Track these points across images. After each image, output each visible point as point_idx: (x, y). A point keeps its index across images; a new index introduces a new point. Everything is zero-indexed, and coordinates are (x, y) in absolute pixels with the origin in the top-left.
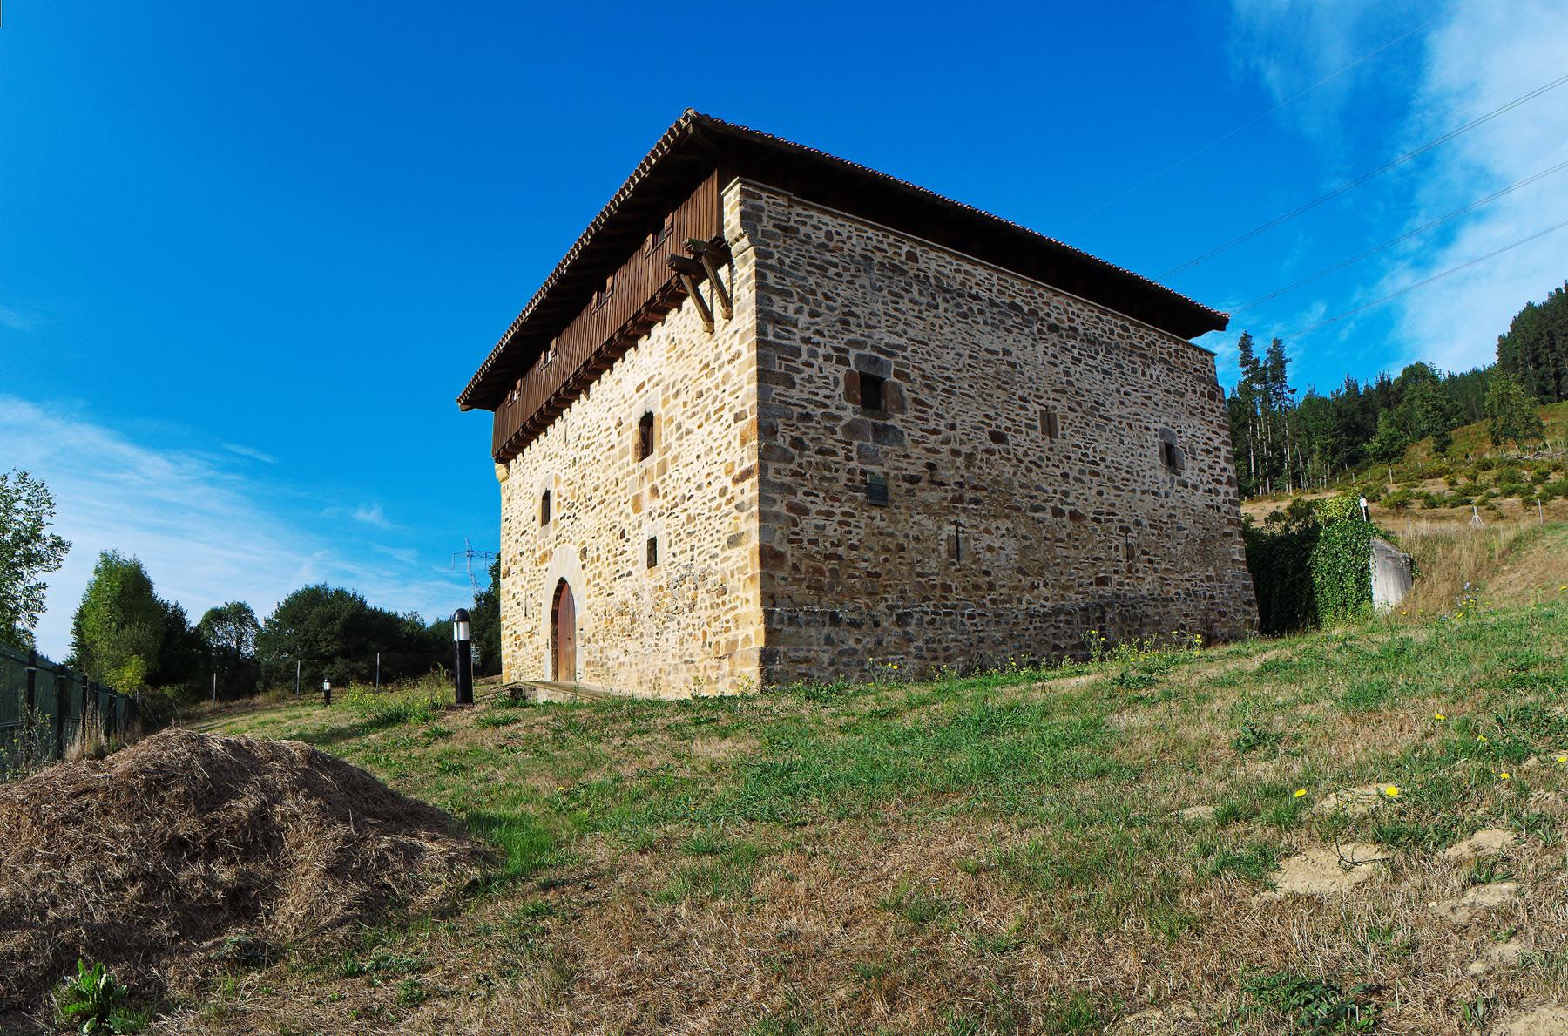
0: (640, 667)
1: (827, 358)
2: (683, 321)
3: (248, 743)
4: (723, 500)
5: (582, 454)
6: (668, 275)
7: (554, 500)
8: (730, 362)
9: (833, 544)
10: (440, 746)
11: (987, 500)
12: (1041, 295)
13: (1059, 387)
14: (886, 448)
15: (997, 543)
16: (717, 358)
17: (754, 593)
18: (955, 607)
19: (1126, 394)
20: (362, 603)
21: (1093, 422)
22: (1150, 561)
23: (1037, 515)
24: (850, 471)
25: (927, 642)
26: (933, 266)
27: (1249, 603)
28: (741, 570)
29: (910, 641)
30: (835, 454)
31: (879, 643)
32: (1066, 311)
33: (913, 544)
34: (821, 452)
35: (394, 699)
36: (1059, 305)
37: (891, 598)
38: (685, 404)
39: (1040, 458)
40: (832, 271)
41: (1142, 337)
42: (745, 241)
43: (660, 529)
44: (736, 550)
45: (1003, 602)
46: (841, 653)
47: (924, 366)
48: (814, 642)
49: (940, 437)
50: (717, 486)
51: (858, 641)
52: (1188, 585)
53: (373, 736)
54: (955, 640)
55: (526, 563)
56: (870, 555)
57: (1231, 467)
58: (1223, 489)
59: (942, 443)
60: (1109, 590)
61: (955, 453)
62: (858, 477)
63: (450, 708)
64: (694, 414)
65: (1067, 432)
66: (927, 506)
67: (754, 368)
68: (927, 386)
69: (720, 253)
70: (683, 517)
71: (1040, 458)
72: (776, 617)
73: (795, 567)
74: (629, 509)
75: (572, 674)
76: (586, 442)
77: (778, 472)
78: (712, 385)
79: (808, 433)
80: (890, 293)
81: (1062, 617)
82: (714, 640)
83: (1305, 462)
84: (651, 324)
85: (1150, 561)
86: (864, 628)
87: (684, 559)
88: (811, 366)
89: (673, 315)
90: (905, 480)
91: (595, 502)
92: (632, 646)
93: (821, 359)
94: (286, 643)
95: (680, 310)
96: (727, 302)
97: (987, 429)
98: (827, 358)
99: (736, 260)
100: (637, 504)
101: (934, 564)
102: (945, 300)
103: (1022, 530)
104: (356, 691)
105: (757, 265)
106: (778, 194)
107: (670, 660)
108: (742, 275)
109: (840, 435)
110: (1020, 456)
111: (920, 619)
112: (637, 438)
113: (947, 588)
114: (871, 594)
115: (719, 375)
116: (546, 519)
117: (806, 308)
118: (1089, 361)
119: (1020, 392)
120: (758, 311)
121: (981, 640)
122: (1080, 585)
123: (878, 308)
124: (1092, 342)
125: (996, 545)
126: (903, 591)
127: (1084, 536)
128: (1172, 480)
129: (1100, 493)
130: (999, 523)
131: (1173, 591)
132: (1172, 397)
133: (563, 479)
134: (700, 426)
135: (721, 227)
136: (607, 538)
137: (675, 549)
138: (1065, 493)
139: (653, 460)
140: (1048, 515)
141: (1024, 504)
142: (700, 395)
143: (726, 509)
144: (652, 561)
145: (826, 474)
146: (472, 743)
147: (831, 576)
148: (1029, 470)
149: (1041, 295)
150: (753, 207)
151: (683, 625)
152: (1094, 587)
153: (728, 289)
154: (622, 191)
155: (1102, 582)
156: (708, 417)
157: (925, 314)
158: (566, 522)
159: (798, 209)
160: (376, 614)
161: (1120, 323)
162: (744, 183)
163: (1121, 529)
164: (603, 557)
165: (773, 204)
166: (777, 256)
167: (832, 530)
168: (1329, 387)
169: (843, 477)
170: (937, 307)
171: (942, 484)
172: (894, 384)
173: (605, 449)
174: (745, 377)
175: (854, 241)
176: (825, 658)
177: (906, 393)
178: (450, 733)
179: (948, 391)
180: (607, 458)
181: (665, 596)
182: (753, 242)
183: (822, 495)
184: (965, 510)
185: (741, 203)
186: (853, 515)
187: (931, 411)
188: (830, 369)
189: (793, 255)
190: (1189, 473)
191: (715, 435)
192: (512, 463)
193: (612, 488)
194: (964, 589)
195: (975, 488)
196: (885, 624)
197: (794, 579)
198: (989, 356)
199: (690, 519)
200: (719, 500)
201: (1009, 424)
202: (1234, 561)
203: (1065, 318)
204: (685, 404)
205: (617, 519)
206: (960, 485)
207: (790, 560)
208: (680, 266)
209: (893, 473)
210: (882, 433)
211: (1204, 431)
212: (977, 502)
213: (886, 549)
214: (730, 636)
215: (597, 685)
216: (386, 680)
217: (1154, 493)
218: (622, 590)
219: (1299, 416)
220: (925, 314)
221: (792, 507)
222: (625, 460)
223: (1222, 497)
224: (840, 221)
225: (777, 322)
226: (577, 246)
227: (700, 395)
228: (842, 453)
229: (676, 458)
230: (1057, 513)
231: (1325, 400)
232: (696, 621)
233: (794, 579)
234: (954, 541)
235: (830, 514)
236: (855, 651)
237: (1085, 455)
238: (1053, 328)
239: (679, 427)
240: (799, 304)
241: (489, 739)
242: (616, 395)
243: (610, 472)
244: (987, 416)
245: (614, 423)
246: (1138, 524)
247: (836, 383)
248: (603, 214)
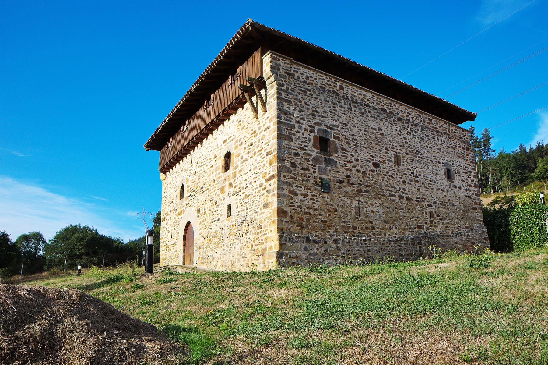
0: (222, 259)
1: (306, 130)
2: (245, 113)
3: (44, 290)
4: (261, 188)
5: (199, 169)
6: (239, 92)
7: (186, 189)
8: (265, 130)
9: (307, 208)
10: (139, 293)
11: (371, 191)
12: (395, 105)
13: (402, 144)
14: (330, 168)
15: (375, 210)
16: (259, 129)
17: (274, 228)
18: (358, 236)
19: (430, 148)
20: (96, 232)
21: (416, 159)
22: (441, 219)
23: (392, 198)
24: (315, 178)
25: (346, 251)
26: (350, 92)
27: (485, 239)
28: (269, 218)
29: (339, 250)
30: (309, 170)
31: (326, 250)
32: (405, 112)
33: (341, 209)
34: (303, 169)
35: (111, 273)
36: (403, 110)
37: (332, 231)
38: (245, 148)
39: (394, 174)
40: (308, 93)
41: (437, 124)
42: (272, 79)
43: (232, 200)
44: (267, 210)
45: (378, 235)
46: (311, 255)
47: (346, 134)
48: (298, 250)
49: (352, 164)
50: (258, 183)
51: (318, 249)
52: (457, 230)
53: (105, 288)
54: (358, 250)
55: (173, 215)
56: (323, 213)
57: (476, 180)
58: (472, 189)
59: (353, 167)
60: (422, 231)
61: (358, 171)
62: (318, 180)
63: (143, 275)
64: (249, 153)
65: (405, 163)
66: (346, 193)
67: (276, 133)
68: (347, 142)
69: (262, 83)
70: (243, 196)
71: (394, 174)
72: (283, 238)
73: (292, 217)
74: (219, 192)
75: (192, 262)
76: (200, 164)
77: (285, 177)
78: (257, 140)
79: (298, 161)
80: (332, 103)
81: (403, 242)
82: (256, 248)
83: (498, 181)
84: (230, 115)
85: (441, 219)
86: (320, 244)
87: (243, 213)
88: (300, 133)
89: (240, 111)
90: (337, 182)
91: (204, 189)
92: (219, 250)
93: (303, 130)
94: (60, 249)
95: (243, 108)
96: (264, 105)
97: (372, 161)
98: (306, 130)
99: (268, 87)
100: (223, 190)
101: (349, 217)
102: (355, 107)
103: (386, 204)
104: (94, 269)
105: (278, 89)
106: (286, 59)
107: (236, 256)
108: (271, 93)
109: (311, 162)
110: (385, 173)
111: (343, 241)
112: (223, 163)
113: (354, 228)
114: (323, 230)
115: (260, 136)
116: (182, 196)
117: (298, 108)
118: (414, 133)
119: (385, 146)
120: (278, 109)
121: (369, 251)
122: (410, 229)
123: (327, 109)
124: (416, 126)
125: (375, 210)
126: (336, 229)
127: (412, 207)
128: (450, 185)
129: (419, 189)
130: (376, 201)
131: (451, 232)
132: (450, 149)
133: (190, 179)
134: (251, 158)
135: (262, 73)
136: (209, 204)
137: (239, 209)
138: (404, 189)
139: (230, 172)
140: (397, 198)
141: (387, 193)
142: (252, 144)
143: (262, 192)
144: (229, 214)
145: (305, 178)
146: (155, 291)
147: (307, 222)
148: (389, 179)
149: (395, 105)
150: (276, 64)
151: (242, 241)
152: (416, 230)
153: (264, 99)
154: (219, 56)
155: (420, 227)
156: (255, 154)
157: (346, 112)
158: (191, 198)
159: (294, 66)
160: (102, 237)
161: (428, 117)
162: (273, 53)
163: (428, 205)
164: (207, 213)
165: (285, 63)
166: (286, 85)
167: (307, 202)
168: (512, 148)
169: (312, 180)
170: (351, 110)
171: (352, 184)
172: (333, 142)
173: (209, 167)
174: (272, 137)
175: (317, 80)
176: (304, 256)
177: (338, 145)
178: (144, 286)
179: (355, 145)
180: (210, 171)
181: (235, 229)
182: (276, 79)
183: (303, 187)
184: (362, 195)
185: (271, 62)
186: (316, 196)
187: (348, 153)
188: (307, 134)
189: (292, 85)
190: (457, 181)
191: (258, 161)
192: (168, 173)
193: (212, 183)
194: (362, 229)
195: (366, 186)
196: (329, 243)
197: (291, 222)
198: (373, 131)
199: (246, 196)
200: (259, 188)
201: (381, 159)
202: (478, 220)
203: (404, 115)
204: (245, 148)
205: (214, 196)
206: (360, 184)
207: (290, 214)
208: (244, 89)
209: (332, 179)
210: (328, 162)
211: (464, 164)
212: (367, 192)
213: (330, 211)
214: (263, 246)
215: (204, 267)
216: (106, 265)
217: (442, 190)
218: (215, 227)
219: (496, 161)
220: (346, 112)
221: (290, 192)
222: (218, 172)
223: (472, 192)
224: (312, 71)
225: (285, 114)
226: (198, 80)
227: (252, 144)
228: (312, 170)
229: (240, 171)
230: (401, 197)
231: (509, 154)
232: (248, 240)
233: (291, 222)
234: (357, 208)
235: (306, 195)
236: (316, 254)
237: (413, 173)
238: (400, 119)
239: (242, 158)
240: (294, 106)
241: (163, 289)
242: (214, 145)
243: (211, 177)
244: (371, 156)
245: (213, 156)
246: (435, 203)
247: (310, 140)
248: (210, 66)
